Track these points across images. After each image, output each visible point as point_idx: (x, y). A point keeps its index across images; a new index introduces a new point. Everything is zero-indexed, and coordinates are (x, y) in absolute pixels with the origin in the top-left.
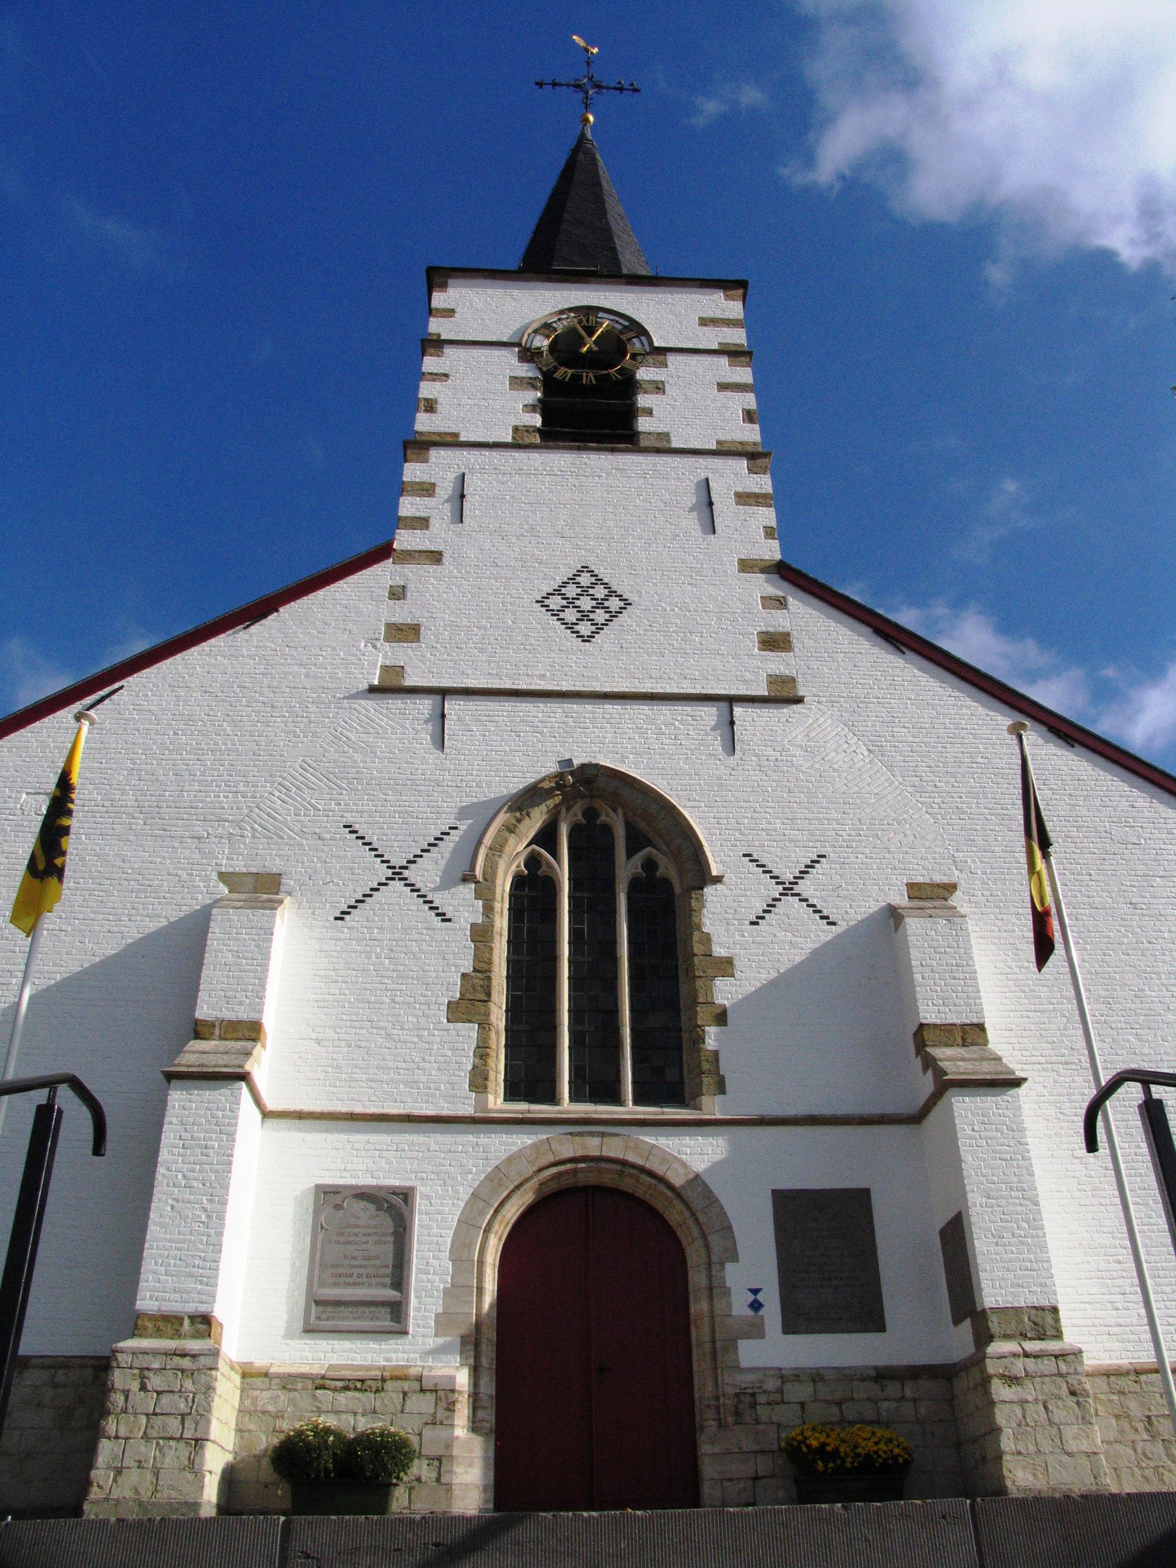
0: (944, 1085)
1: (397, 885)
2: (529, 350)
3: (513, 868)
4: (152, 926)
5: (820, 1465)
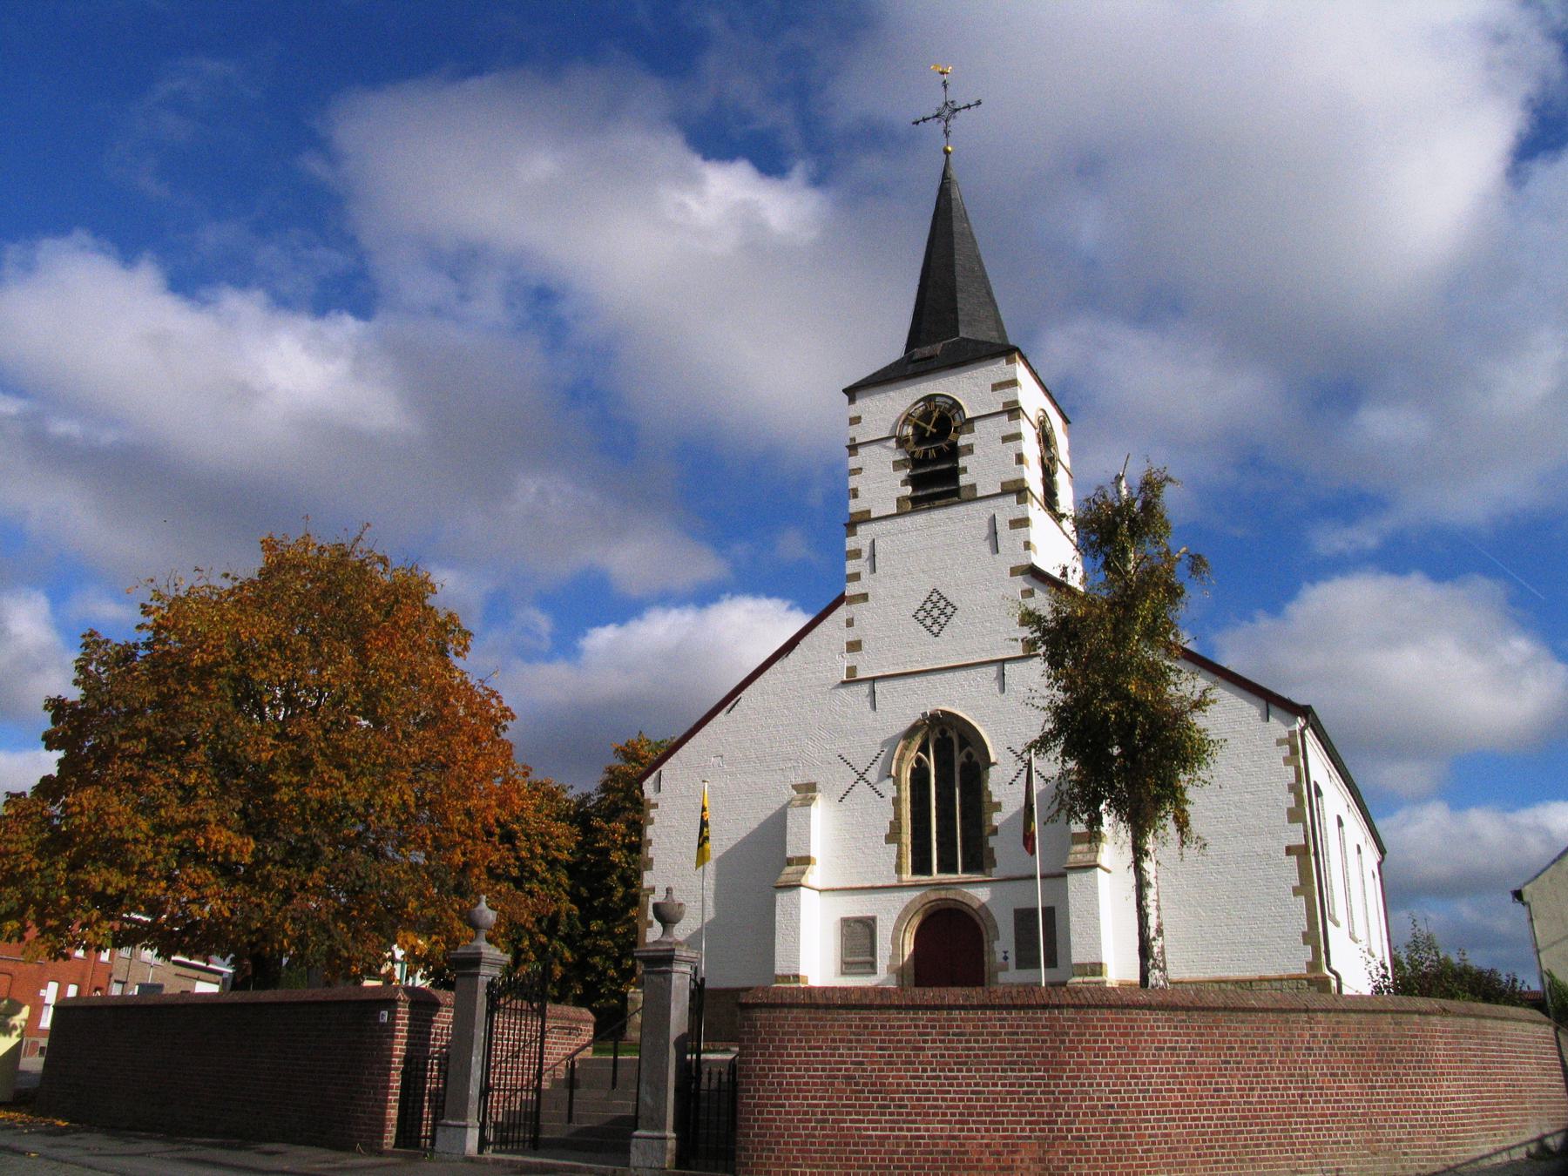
4: (770, 813)
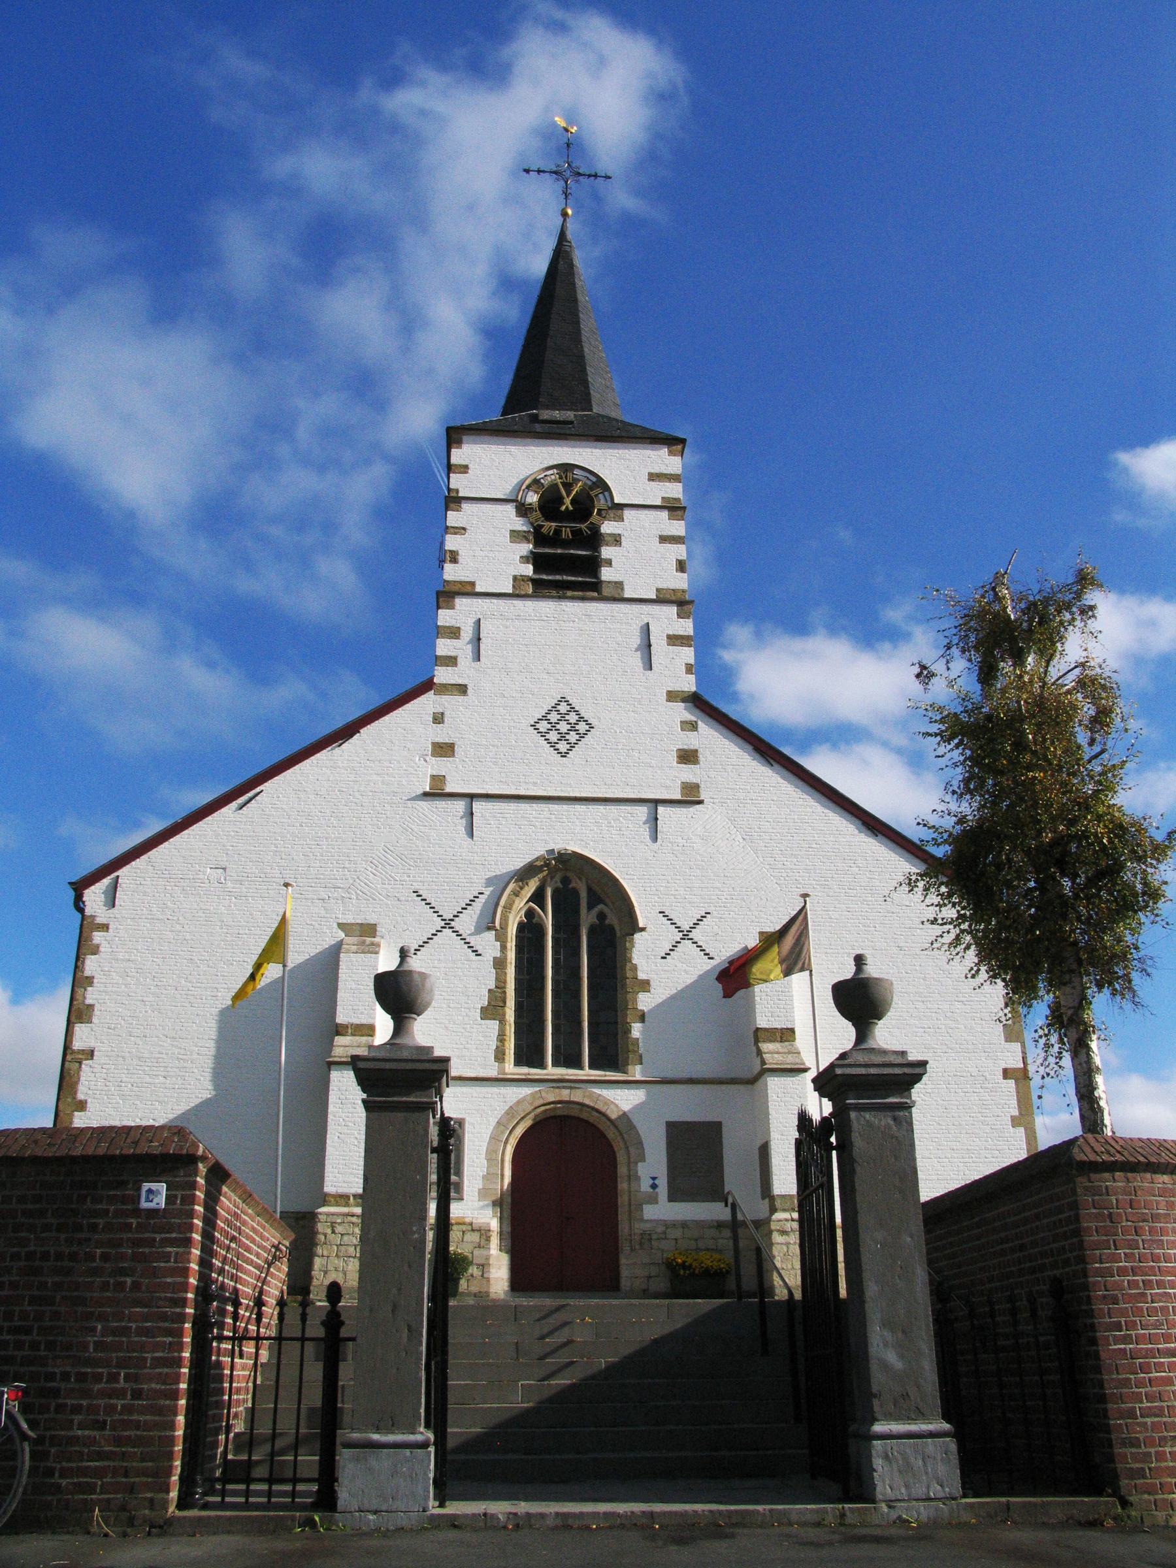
0: (766, 1071)
1: (447, 931)
2: (523, 505)
3: (518, 919)
5: (682, 1272)
